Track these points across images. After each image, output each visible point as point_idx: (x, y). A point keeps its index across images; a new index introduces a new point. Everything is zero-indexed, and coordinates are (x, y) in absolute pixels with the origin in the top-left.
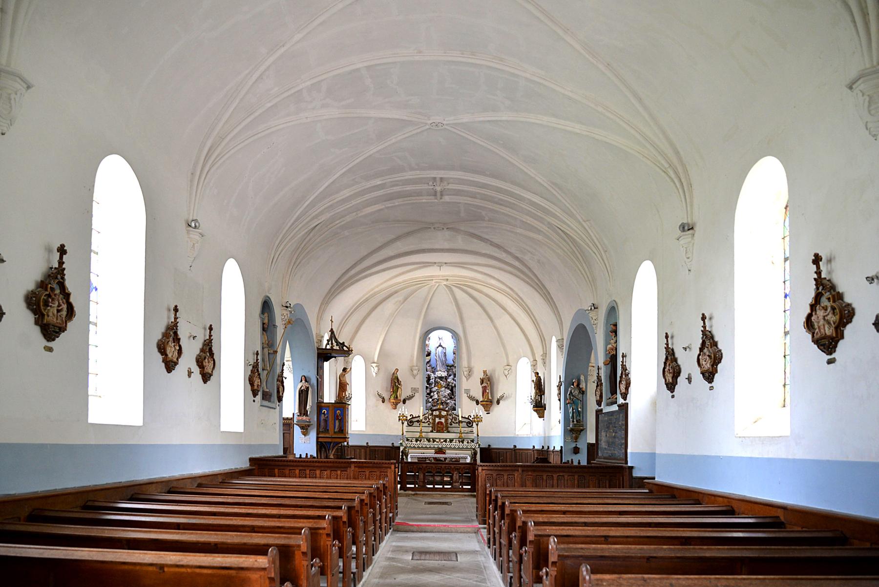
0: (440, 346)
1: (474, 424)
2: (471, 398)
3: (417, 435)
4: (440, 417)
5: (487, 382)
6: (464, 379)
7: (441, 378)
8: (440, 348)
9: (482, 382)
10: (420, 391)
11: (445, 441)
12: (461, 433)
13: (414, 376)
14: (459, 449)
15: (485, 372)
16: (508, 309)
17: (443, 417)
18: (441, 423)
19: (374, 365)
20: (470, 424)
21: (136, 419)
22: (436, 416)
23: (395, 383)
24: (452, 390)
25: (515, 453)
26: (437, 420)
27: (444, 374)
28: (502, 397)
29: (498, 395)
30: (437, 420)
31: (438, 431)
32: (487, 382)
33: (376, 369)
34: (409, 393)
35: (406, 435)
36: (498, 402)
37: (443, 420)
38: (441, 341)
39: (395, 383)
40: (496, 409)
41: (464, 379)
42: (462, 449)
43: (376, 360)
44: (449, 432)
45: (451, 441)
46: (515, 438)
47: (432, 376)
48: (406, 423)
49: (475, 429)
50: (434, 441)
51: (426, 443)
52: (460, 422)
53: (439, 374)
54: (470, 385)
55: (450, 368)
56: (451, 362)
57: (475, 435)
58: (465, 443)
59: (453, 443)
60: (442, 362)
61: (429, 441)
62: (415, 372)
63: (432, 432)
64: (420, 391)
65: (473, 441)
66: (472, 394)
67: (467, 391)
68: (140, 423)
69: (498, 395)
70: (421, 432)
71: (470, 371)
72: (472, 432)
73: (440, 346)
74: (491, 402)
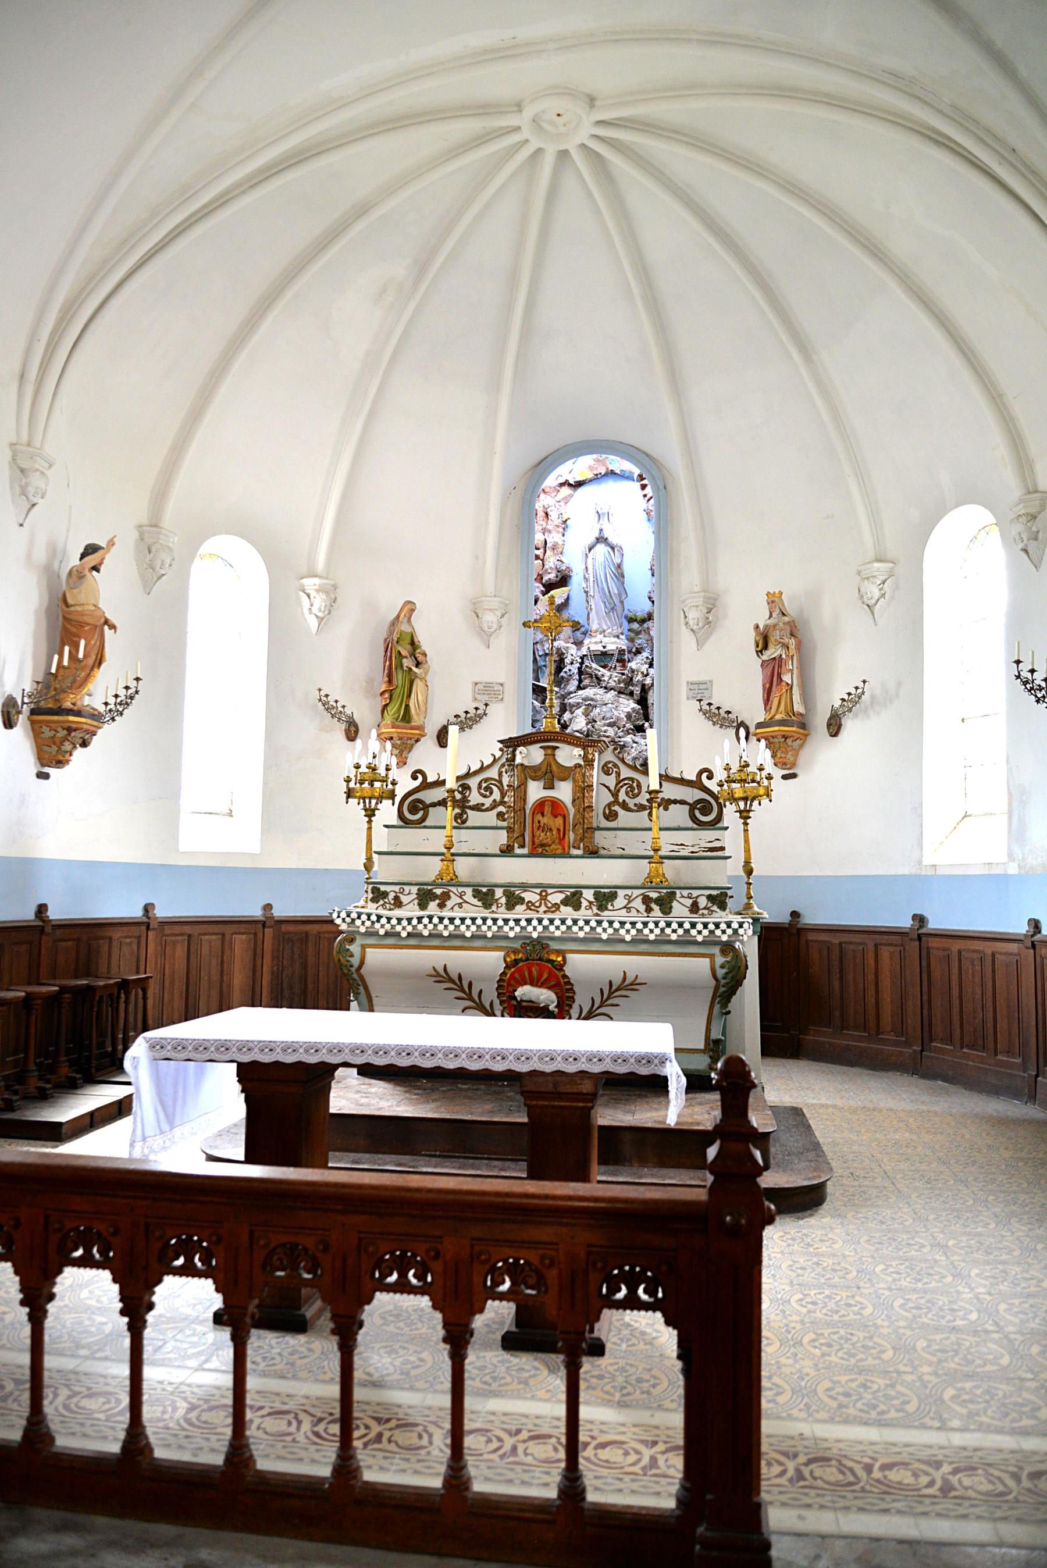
0: (601, 539)
1: (730, 814)
2: (719, 717)
3: (431, 869)
4: (549, 773)
5: (783, 645)
6: (686, 641)
7: (602, 657)
8: (601, 548)
9: (763, 642)
10: (510, 691)
11: (573, 900)
12: (656, 857)
13: (486, 636)
14: (640, 945)
15: (774, 601)
16: (916, 143)
17: (566, 774)
18: (556, 806)
19: (311, 584)
20: (705, 811)
21: (256, 849)
22: (530, 772)
23: (401, 661)
24: (643, 701)
25: (925, 956)
26: (535, 791)
27: (613, 645)
28: (852, 701)
29: (832, 694)
30: (535, 791)
31: (539, 850)
32: (783, 645)
33: (319, 601)
34: (465, 703)
35: (385, 871)
36: (835, 727)
37: (564, 792)
38: (602, 523)
39: (401, 661)
40: (825, 760)
41: (686, 641)
42: (660, 946)
43: (320, 564)
44: (593, 853)
45: (604, 898)
46: (921, 882)
47: (573, 653)
48: (387, 812)
49: (731, 837)
50: (513, 901)
51: (473, 909)
52: (657, 801)
53: (593, 644)
54: (714, 663)
55: (639, 624)
56: (639, 605)
57: (734, 867)
58: (680, 909)
59: (616, 912)
60: (607, 597)
61: (486, 897)
62: (490, 618)
63: (507, 851)
64: (510, 691)
65: (720, 900)
66: (722, 698)
67: (700, 692)
68: (258, 851)
69: (832, 694)
70: (449, 855)
71: (712, 605)
72: (716, 852)
73: (601, 539)
74: (803, 725)
